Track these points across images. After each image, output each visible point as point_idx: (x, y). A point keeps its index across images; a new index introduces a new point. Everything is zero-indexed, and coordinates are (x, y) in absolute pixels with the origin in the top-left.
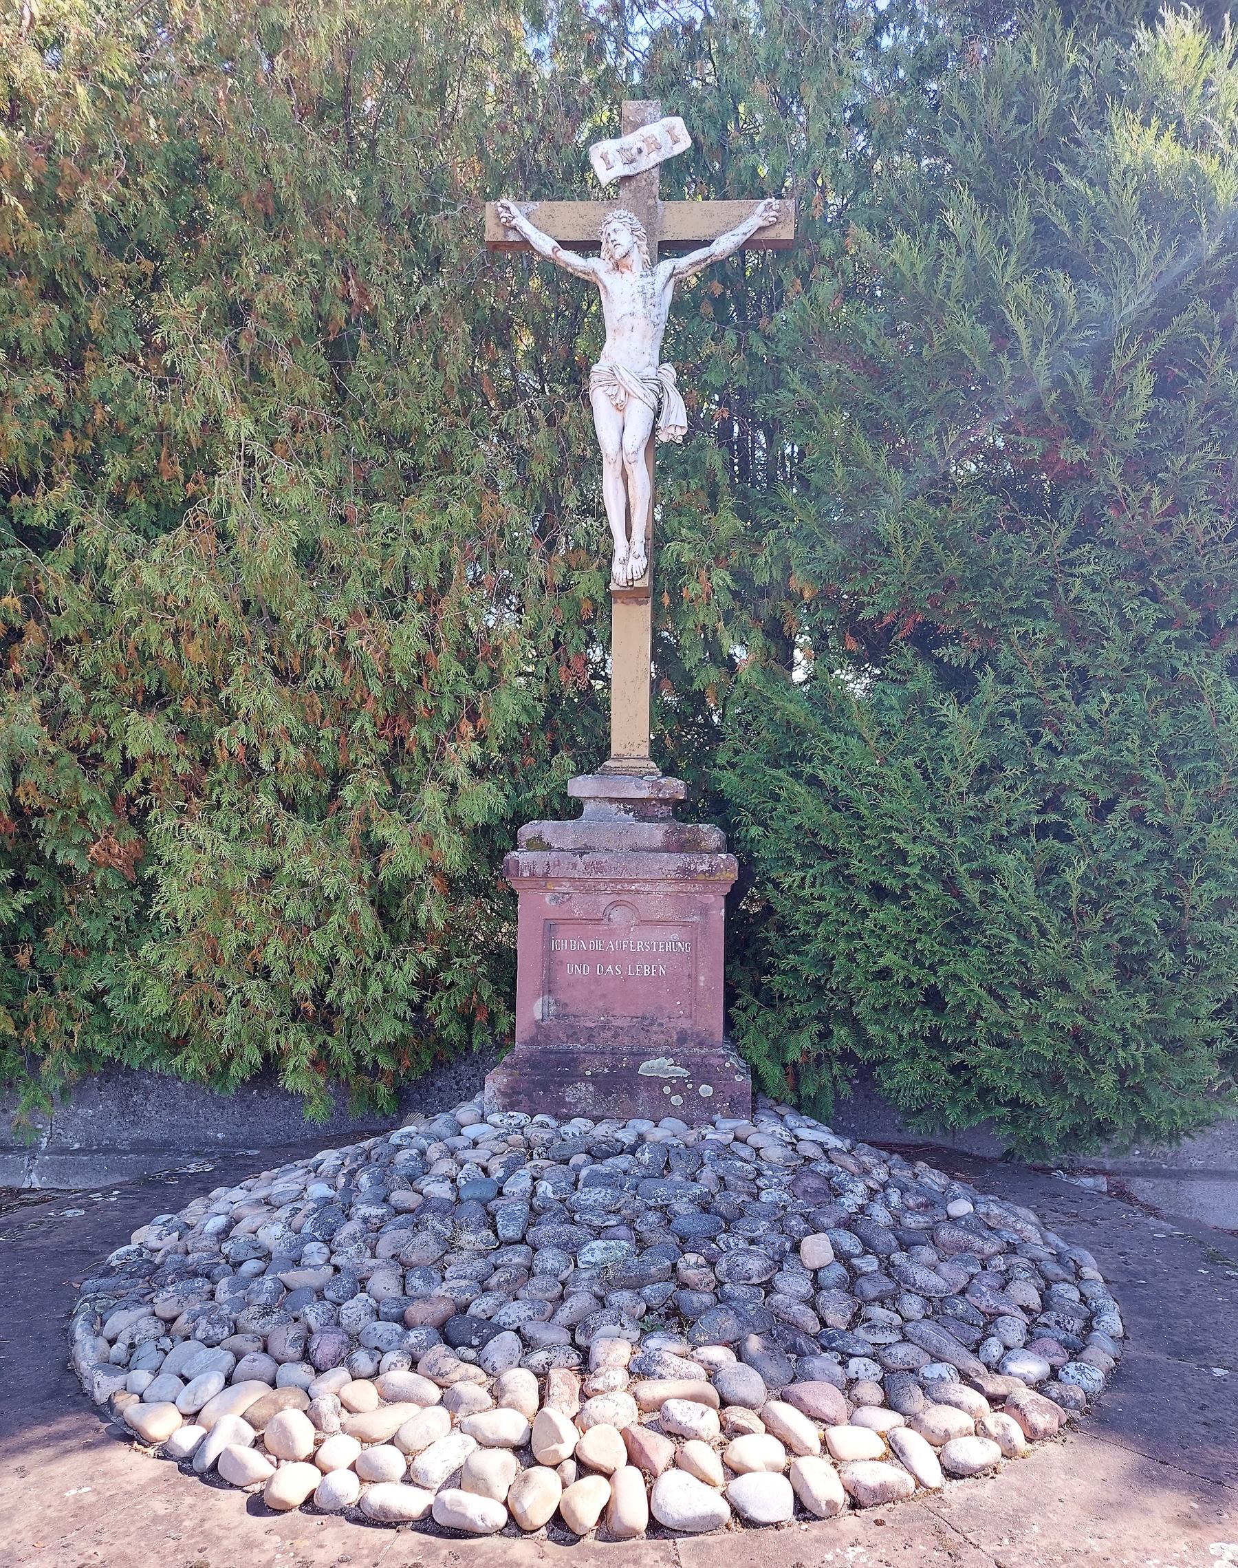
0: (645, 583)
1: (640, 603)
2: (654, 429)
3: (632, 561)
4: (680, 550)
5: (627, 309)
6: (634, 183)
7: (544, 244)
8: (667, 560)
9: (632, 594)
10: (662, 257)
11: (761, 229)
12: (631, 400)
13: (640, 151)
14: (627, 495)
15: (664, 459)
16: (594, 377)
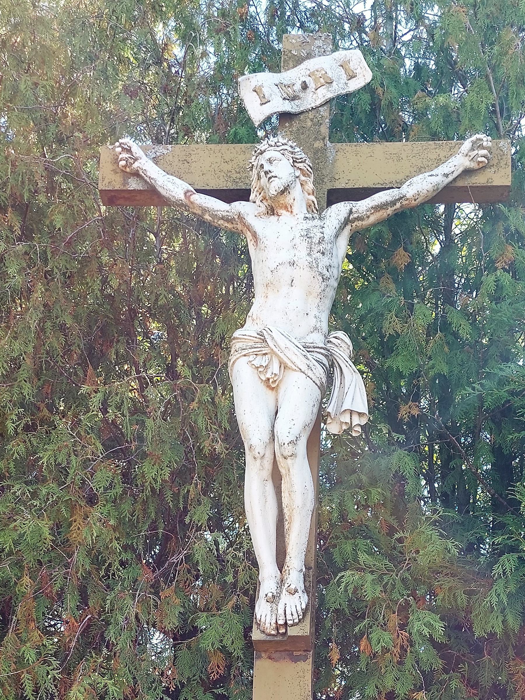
0: (305, 629)
1: (295, 659)
2: (322, 416)
3: (285, 598)
4: (356, 581)
5: (285, 256)
6: (296, 124)
7: (174, 188)
8: (336, 597)
9: (283, 645)
10: (330, 203)
11: (467, 172)
12: (286, 377)
13: (305, 86)
14: (278, 511)
15: (331, 457)
16: (236, 345)
